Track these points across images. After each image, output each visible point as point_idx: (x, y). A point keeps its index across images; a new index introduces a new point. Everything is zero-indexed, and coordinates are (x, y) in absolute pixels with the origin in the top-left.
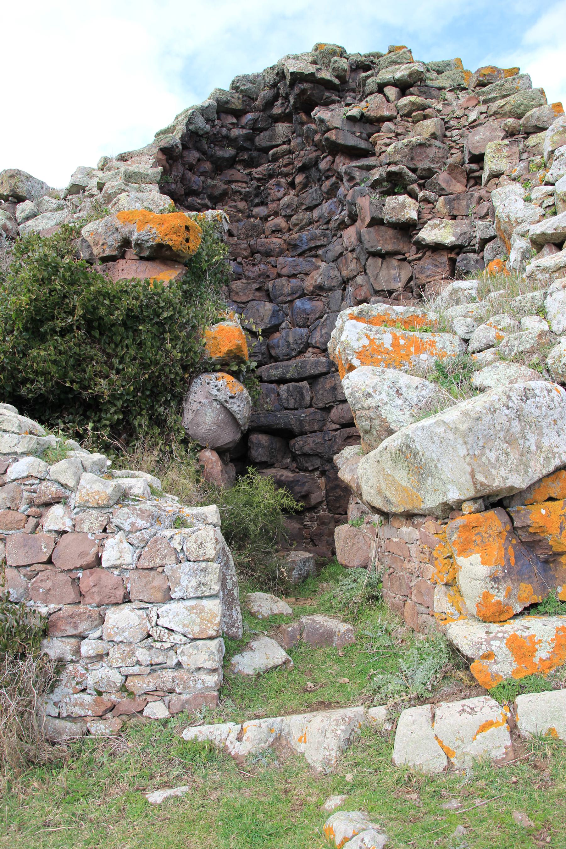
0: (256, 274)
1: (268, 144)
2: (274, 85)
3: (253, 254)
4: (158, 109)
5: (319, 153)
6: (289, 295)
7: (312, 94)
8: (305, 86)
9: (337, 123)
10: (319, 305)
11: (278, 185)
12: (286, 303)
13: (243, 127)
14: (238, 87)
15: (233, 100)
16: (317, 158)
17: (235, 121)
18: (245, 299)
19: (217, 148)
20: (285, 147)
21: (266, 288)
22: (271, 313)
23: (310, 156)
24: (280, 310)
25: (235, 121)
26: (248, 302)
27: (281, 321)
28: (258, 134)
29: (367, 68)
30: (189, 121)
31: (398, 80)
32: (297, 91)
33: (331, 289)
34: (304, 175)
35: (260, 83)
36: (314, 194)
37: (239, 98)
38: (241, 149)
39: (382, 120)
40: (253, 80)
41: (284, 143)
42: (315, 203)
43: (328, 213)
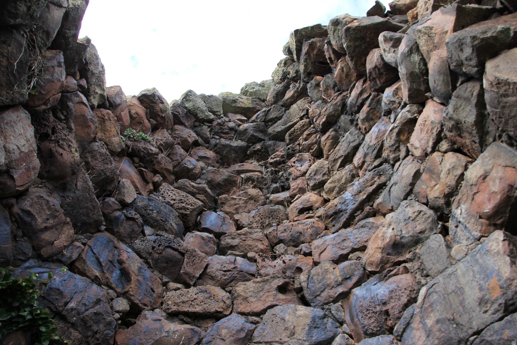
0: (277, 268)
3: (272, 246)
6: (340, 284)
10: (403, 280)
11: (300, 160)
12: (335, 301)
14: (247, 91)
18: (258, 307)
21: (297, 285)
22: (308, 321)
24: (325, 316)
26: (264, 311)
27: (331, 334)
33: (417, 240)
41: (301, 118)
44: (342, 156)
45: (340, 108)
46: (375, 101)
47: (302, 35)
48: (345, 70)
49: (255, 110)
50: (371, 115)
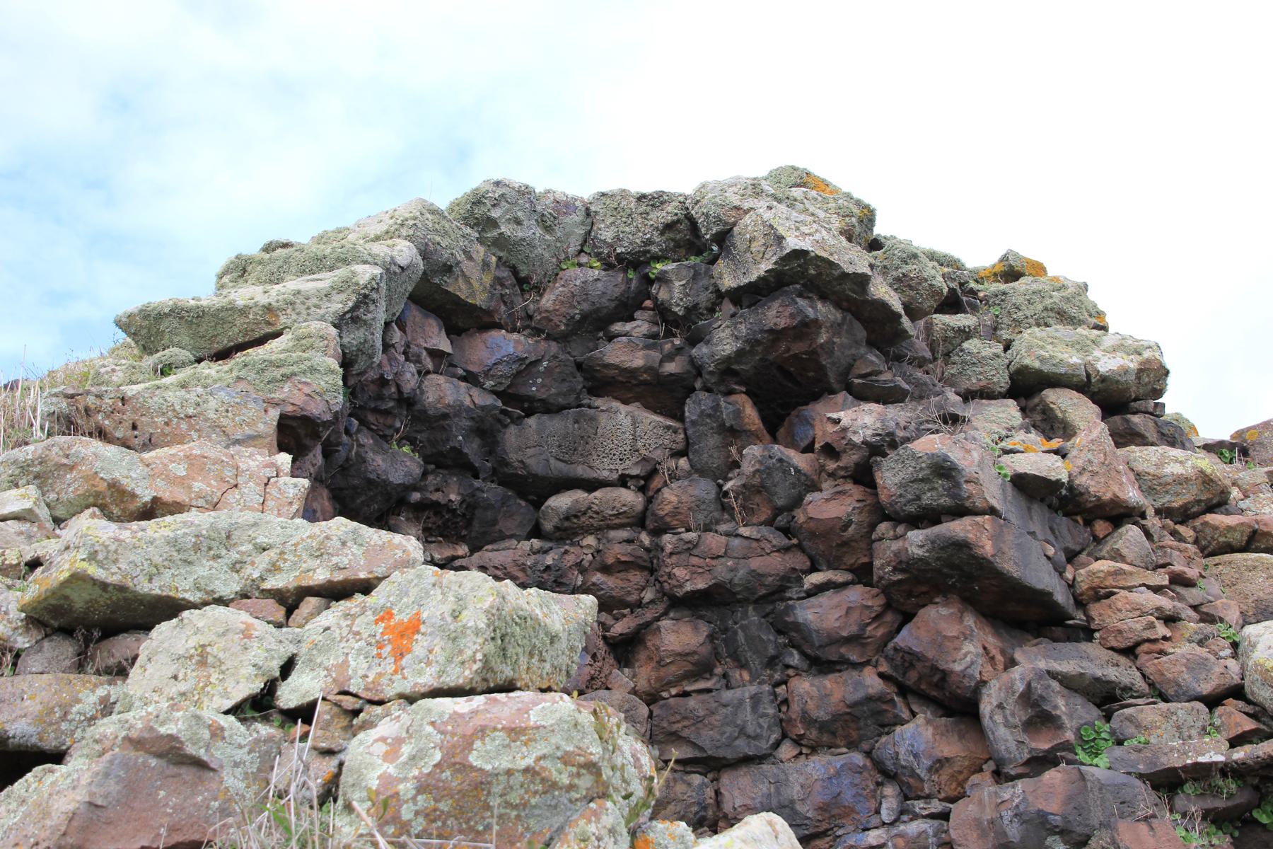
1: (558, 468)
2: (636, 261)
4: (316, 232)
5: (800, 561)
7: (829, 348)
8: (822, 311)
9: (993, 492)
13: (470, 378)
14: (493, 223)
15: (467, 266)
16: (791, 578)
17: (445, 345)
19: (366, 439)
20: (629, 498)
23: (756, 563)
25: (445, 345)
28: (517, 421)
29: (951, 304)
30: (356, 307)
31: (1104, 379)
32: (775, 314)
34: (705, 629)
35: (568, 235)
36: (747, 715)
37: (486, 265)
38: (443, 460)
39: (1120, 515)
40: (551, 212)
41: (623, 481)
42: (744, 747)
43: (823, 808)
44: (701, 749)
45: (763, 592)
46: (873, 706)
47: (804, 274)
48: (851, 530)
49: (486, 319)
50: (838, 725)
